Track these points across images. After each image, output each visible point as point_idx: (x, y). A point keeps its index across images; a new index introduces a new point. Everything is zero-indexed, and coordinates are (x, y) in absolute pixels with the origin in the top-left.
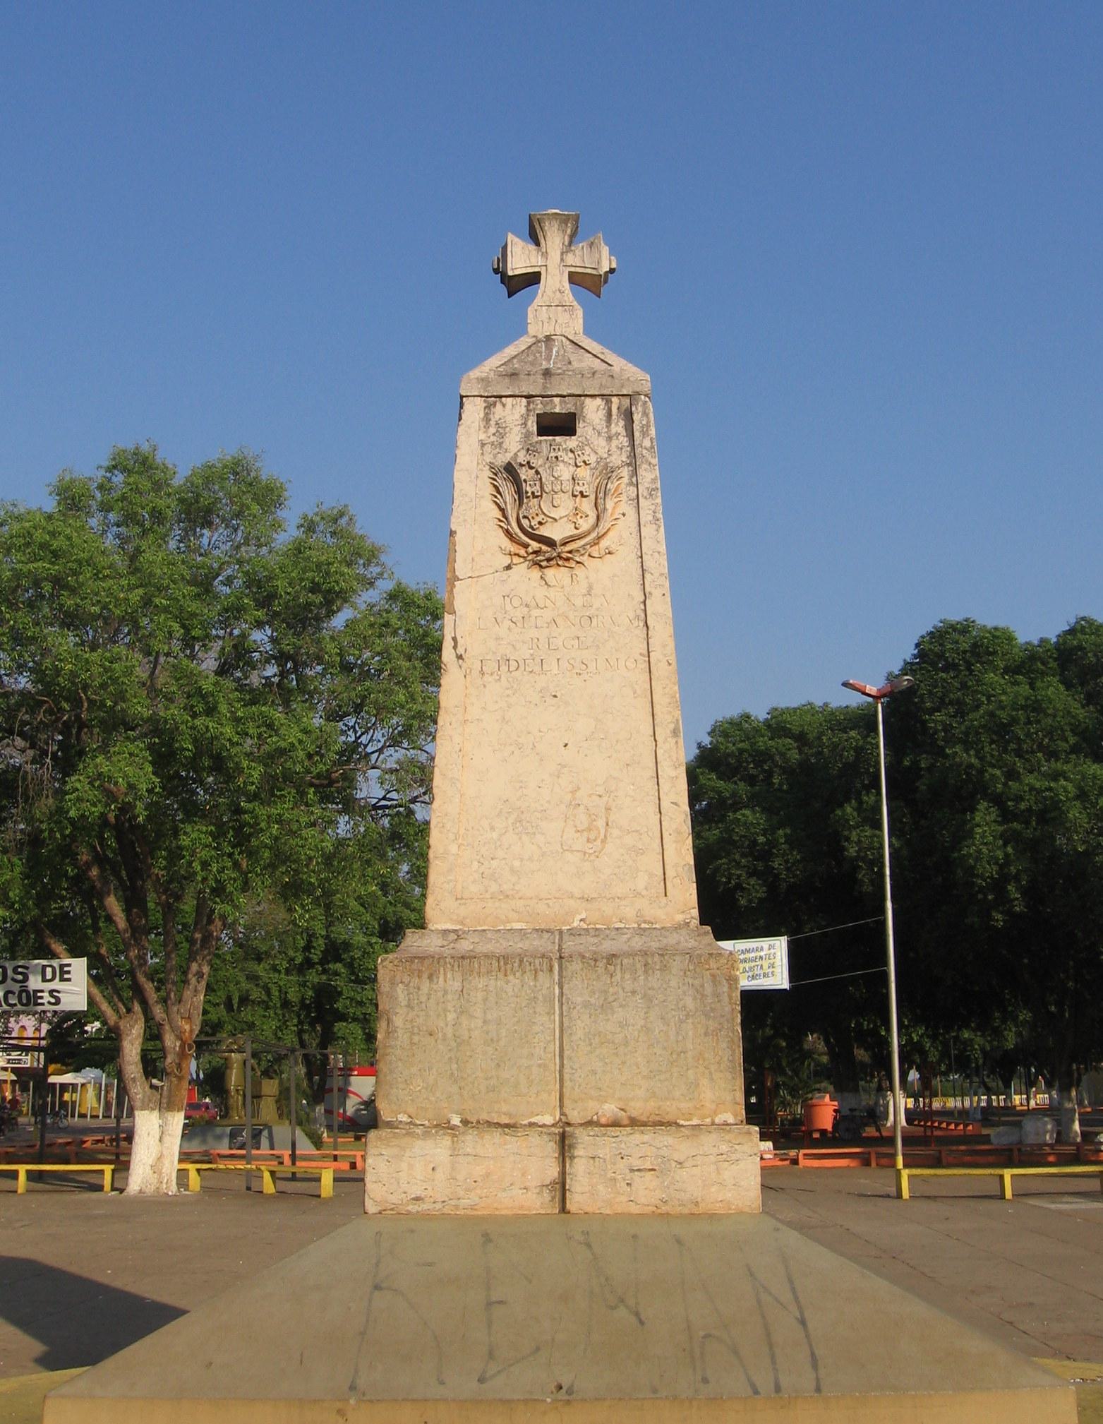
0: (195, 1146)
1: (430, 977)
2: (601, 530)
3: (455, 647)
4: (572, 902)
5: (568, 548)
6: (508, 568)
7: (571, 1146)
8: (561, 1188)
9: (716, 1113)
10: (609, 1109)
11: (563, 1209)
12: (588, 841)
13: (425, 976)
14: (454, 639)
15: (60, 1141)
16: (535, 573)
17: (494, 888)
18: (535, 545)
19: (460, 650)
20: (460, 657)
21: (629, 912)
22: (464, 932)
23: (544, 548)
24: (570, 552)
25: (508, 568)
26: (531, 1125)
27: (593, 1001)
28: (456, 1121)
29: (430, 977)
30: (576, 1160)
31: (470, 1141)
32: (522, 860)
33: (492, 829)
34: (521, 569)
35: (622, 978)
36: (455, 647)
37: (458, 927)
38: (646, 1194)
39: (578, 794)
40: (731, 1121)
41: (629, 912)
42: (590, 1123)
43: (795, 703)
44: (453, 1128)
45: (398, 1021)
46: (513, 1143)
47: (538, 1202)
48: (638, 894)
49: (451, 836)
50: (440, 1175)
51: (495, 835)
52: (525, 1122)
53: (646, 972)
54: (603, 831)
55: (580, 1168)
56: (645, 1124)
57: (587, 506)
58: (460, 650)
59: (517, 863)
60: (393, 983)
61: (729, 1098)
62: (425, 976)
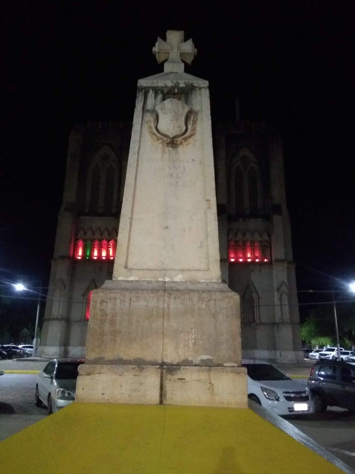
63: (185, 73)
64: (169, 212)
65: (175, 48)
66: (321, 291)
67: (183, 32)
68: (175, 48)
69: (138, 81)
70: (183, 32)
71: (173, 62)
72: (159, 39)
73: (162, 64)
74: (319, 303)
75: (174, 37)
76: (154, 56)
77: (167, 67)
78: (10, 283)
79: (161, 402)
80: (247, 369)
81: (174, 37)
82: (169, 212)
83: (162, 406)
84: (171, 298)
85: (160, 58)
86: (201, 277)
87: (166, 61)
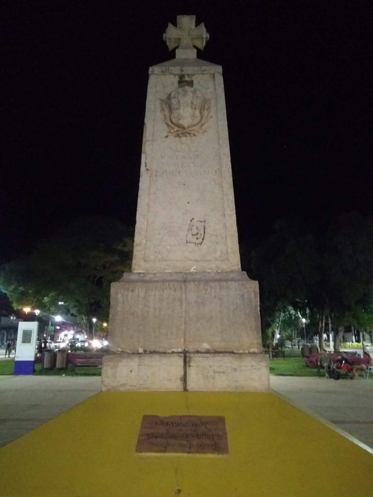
0: (271, 323)
1: (132, 291)
2: (203, 122)
3: (146, 166)
4: (190, 262)
5: (190, 129)
6: (167, 137)
7: (190, 361)
8: (184, 379)
9: (250, 347)
10: (206, 346)
11: (185, 389)
12: (197, 238)
13: (130, 290)
14: (146, 163)
15: (278, 325)
16: (177, 139)
17: (160, 257)
18: (176, 129)
19: (148, 167)
20: (148, 170)
21: (213, 266)
22: (147, 273)
23: (180, 129)
24: (190, 131)
25: (167, 137)
26: (173, 353)
27: (198, 301)
28: (141, 350)
29: (132, 291)
30: (191, 368)
31: (147, 360)
32: (171, 246)
33: (159, 234)
34: (171, 137)
35: (211, 291)
36: (146, 166)
37: (145, 272)
38: (221, 383)
39: (193, 221)
40: (256, 351)
41: (213, 266)
42: (198, 352)
43: (167, 415)
44: (139, 354)
45: (119, 309)
46: (165, 361)
47: (177, 385)
48: (217, 259)
49: (143, 237)
50: (134, 373)
51: (160, 236)
52: (170, 351)
53: (220, 289)
54: (203, 235)
55: (192, 372)
56: (220, 352)
57: (197, 112)
58: (148, 167)
59: (169, 247)
60: (117, 294)
61: (255, 342)
62: (130, 290)
63: (198, 60)
64: (186, 198)
65: (186, 33)
66: (324, 319)
67: (194, 17)
68: (186, 33)
69: (148, 70)
70: (194, 17)
71: (186, 48)
72: (170, 25)
73: (174, 51)
74: (324, 321)
75: (187, 22)
76: (165, 43)
77: (180, 54)
78: (93, 324)
79: (185, 389)
80: (222, 67)
81: (187, 22)
82: (186, 198)
83: (186, 393)
84: (185, 279)
85: (171, 45)
86: (225, 267)
87: (177, 47)
